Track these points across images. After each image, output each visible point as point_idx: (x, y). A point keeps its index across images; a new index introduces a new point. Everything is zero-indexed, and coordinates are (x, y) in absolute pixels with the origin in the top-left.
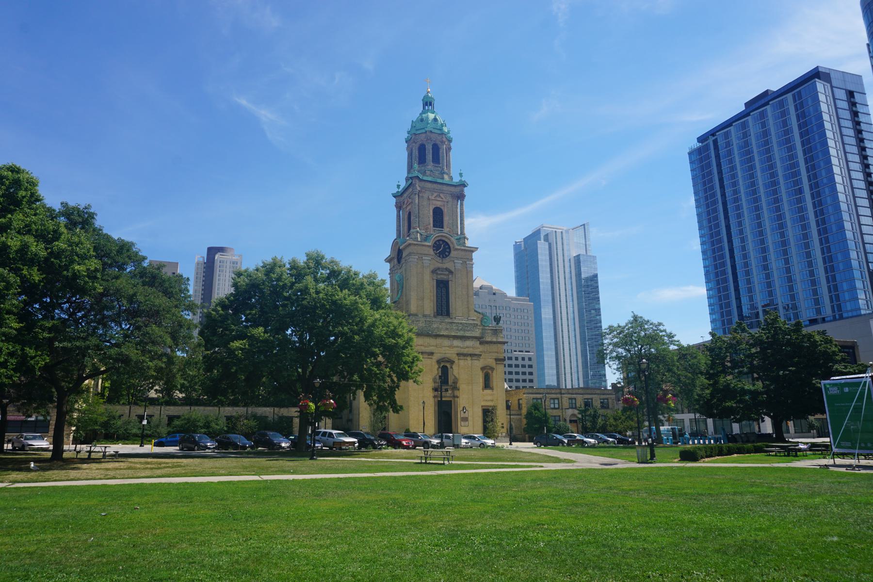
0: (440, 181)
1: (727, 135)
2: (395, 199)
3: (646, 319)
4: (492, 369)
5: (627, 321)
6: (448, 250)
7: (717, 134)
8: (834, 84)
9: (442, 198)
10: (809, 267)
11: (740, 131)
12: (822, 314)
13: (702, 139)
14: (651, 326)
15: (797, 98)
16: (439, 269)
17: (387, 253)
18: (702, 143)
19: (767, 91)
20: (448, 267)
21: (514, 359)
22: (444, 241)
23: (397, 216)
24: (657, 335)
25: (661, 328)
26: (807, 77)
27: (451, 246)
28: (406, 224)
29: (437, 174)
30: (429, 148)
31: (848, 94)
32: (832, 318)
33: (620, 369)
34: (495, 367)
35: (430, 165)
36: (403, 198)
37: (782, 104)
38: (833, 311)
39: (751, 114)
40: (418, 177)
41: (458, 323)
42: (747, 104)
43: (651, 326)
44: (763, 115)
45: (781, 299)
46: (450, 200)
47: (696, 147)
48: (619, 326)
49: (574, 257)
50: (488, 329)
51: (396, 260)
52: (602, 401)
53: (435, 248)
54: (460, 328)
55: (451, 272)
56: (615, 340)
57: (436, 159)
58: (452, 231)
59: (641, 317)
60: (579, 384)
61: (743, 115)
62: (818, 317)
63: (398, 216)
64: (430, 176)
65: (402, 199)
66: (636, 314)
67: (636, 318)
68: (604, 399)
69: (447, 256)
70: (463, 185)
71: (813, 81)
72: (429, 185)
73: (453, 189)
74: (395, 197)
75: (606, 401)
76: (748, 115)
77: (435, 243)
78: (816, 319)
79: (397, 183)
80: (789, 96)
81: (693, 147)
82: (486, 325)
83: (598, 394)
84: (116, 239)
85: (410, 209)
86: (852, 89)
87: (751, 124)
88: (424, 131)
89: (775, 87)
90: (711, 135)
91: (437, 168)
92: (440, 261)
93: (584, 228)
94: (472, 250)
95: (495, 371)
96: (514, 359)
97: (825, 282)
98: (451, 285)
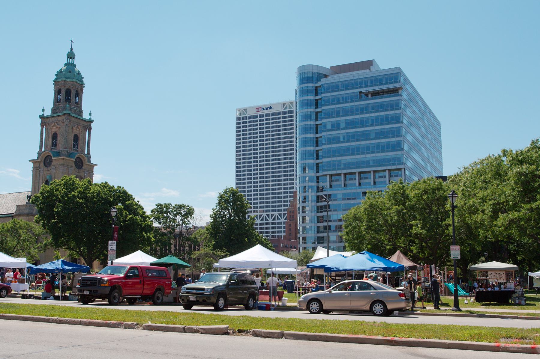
2: (40, 119)
10: (380, 118)
21: (305, 245)
23: (41, 131)
27: (84, 162)
32: (489, 273)
33: (195, 240)
49: (435, 308)
70: (91, 121)
72: (73, 119)
73: (84, 123)
88: (71, 80)
94: (93, 165)
96: (305, 245)
97: (352, 181)
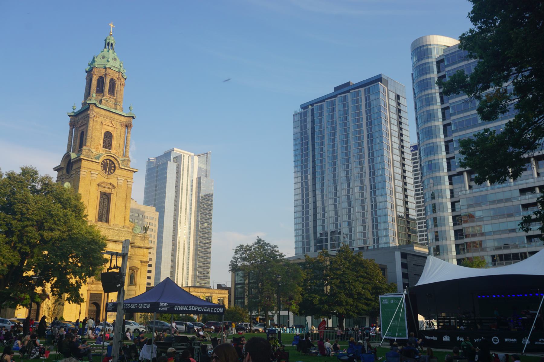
0: (114, 111)
1: (321, 108)
3: (267, 242)
4: (137, 269)
5: (253, 243)
6: (113, 168)
7: (314, 105)
8: (389, 89)
9: (113, 125)
11: (330, 107)
12: (367, 244)
13: (304, 107)
14: (270, 248)
15: (367, 92)
16: (104, 183)
17: (58, 163)
18: (304, 109)
19: (349, 83)
20: (111, 182)
22: (110, 160)
23: (70, 132)
24: (274, 254)
25: (276, 249)
26: (374, 79)
28: (78, 141)
29: (111, 105)
30: (108, 81)
31: (396, 96)
34: (139, 267)
35: (107, 96)
36: (77, 118)
37: (357, 94)
38: (374, 243)
39: (338, 96)
40: (95, 104)
41: (115, 230)
42: (336, 89)
43: (270, 248)
44: (345, 99)
45: (345, 231)
46: (120, 127)
47: (299, 111)
48: (248, 246)
50: (138, 236)
51: (65, 171)
52: (219, 299)
53: (102, 166)
54: (116, 233)
55: (114, 187)
56: (244, 255)
57: (112, 91)
58: (118, 153)
59: (264, 241)
60: (182, 284)
61: (330, 96)
62: (364, 246)
63: (71, 133)
64: (106, 105)
65: (76, 119)
66: (260, 238)
67: (259, 241)
68: (220, 298)
69: (112, 173)
71: (377, 83)
72: (103, 112)
74: (69, 116)
75: (210, 298)
76: (336, 96)
77: (103, 161)
78: (363, 247)
79: (73, 105)
80: (362, 89)
81: (297, 111)
82: (136, 232)
83: (217, 293)
84: (79, 192)
85: (83, 129)
86: (399, 94)
87: (337, 101)
89: (355, 81)
90: (310, 105)
91: (111, 99)
92: (106, 177)
93: (207, 156)
95: (139, 271)
98: (113, 198)
